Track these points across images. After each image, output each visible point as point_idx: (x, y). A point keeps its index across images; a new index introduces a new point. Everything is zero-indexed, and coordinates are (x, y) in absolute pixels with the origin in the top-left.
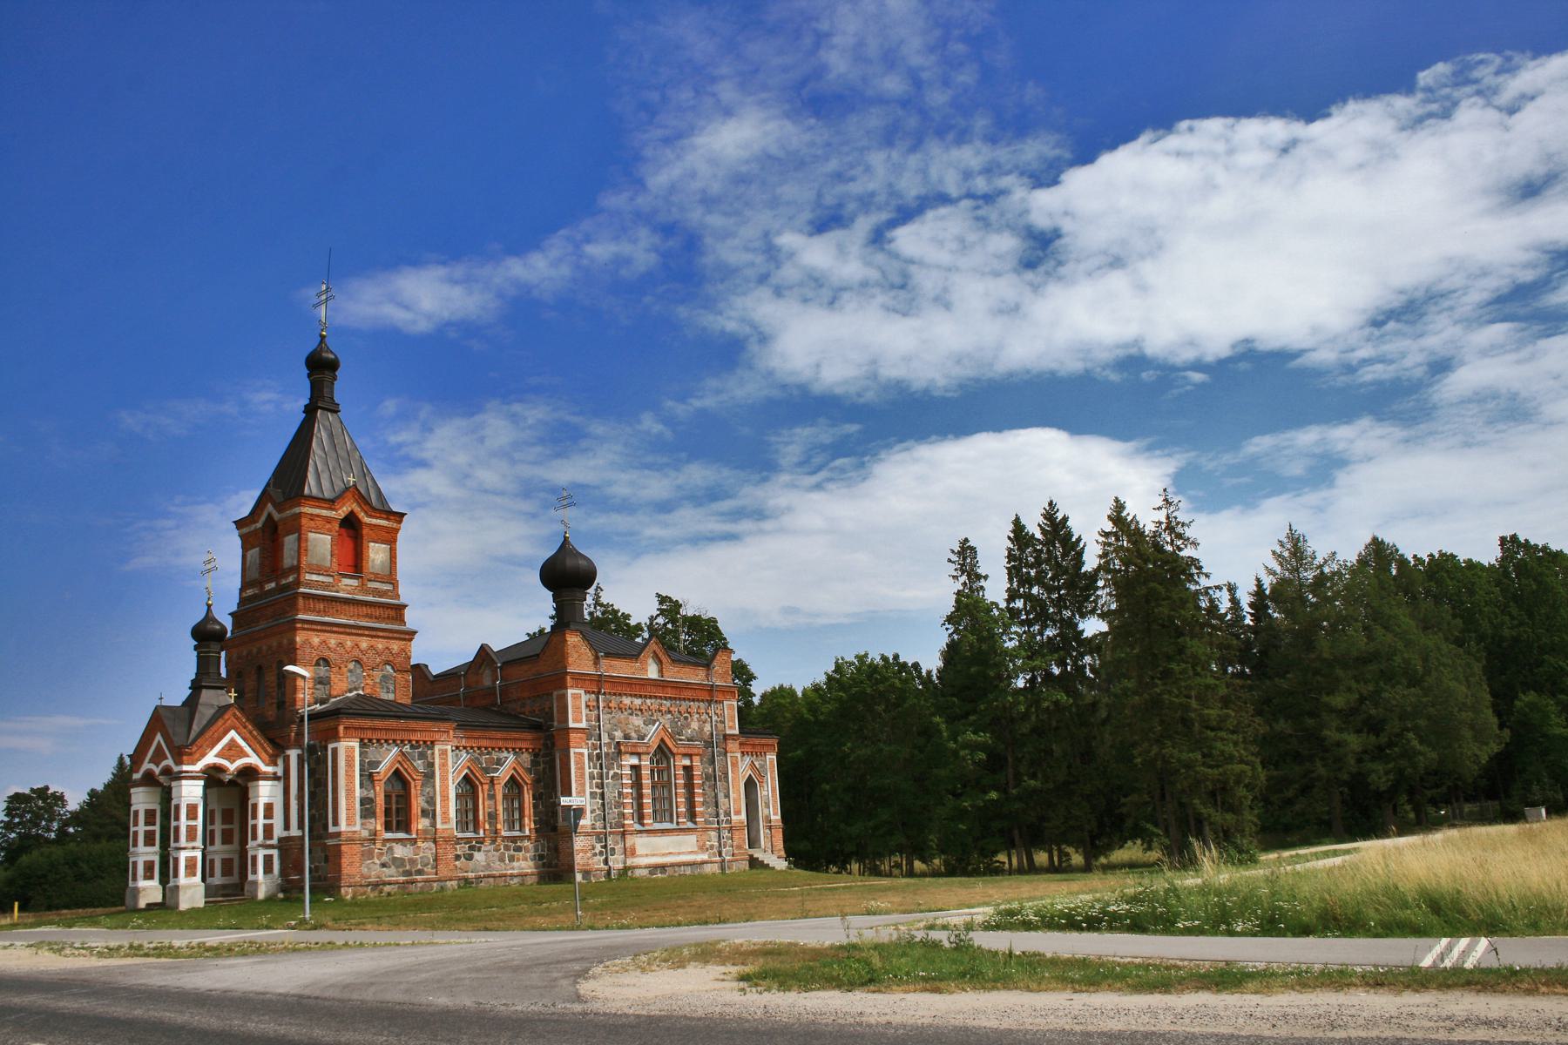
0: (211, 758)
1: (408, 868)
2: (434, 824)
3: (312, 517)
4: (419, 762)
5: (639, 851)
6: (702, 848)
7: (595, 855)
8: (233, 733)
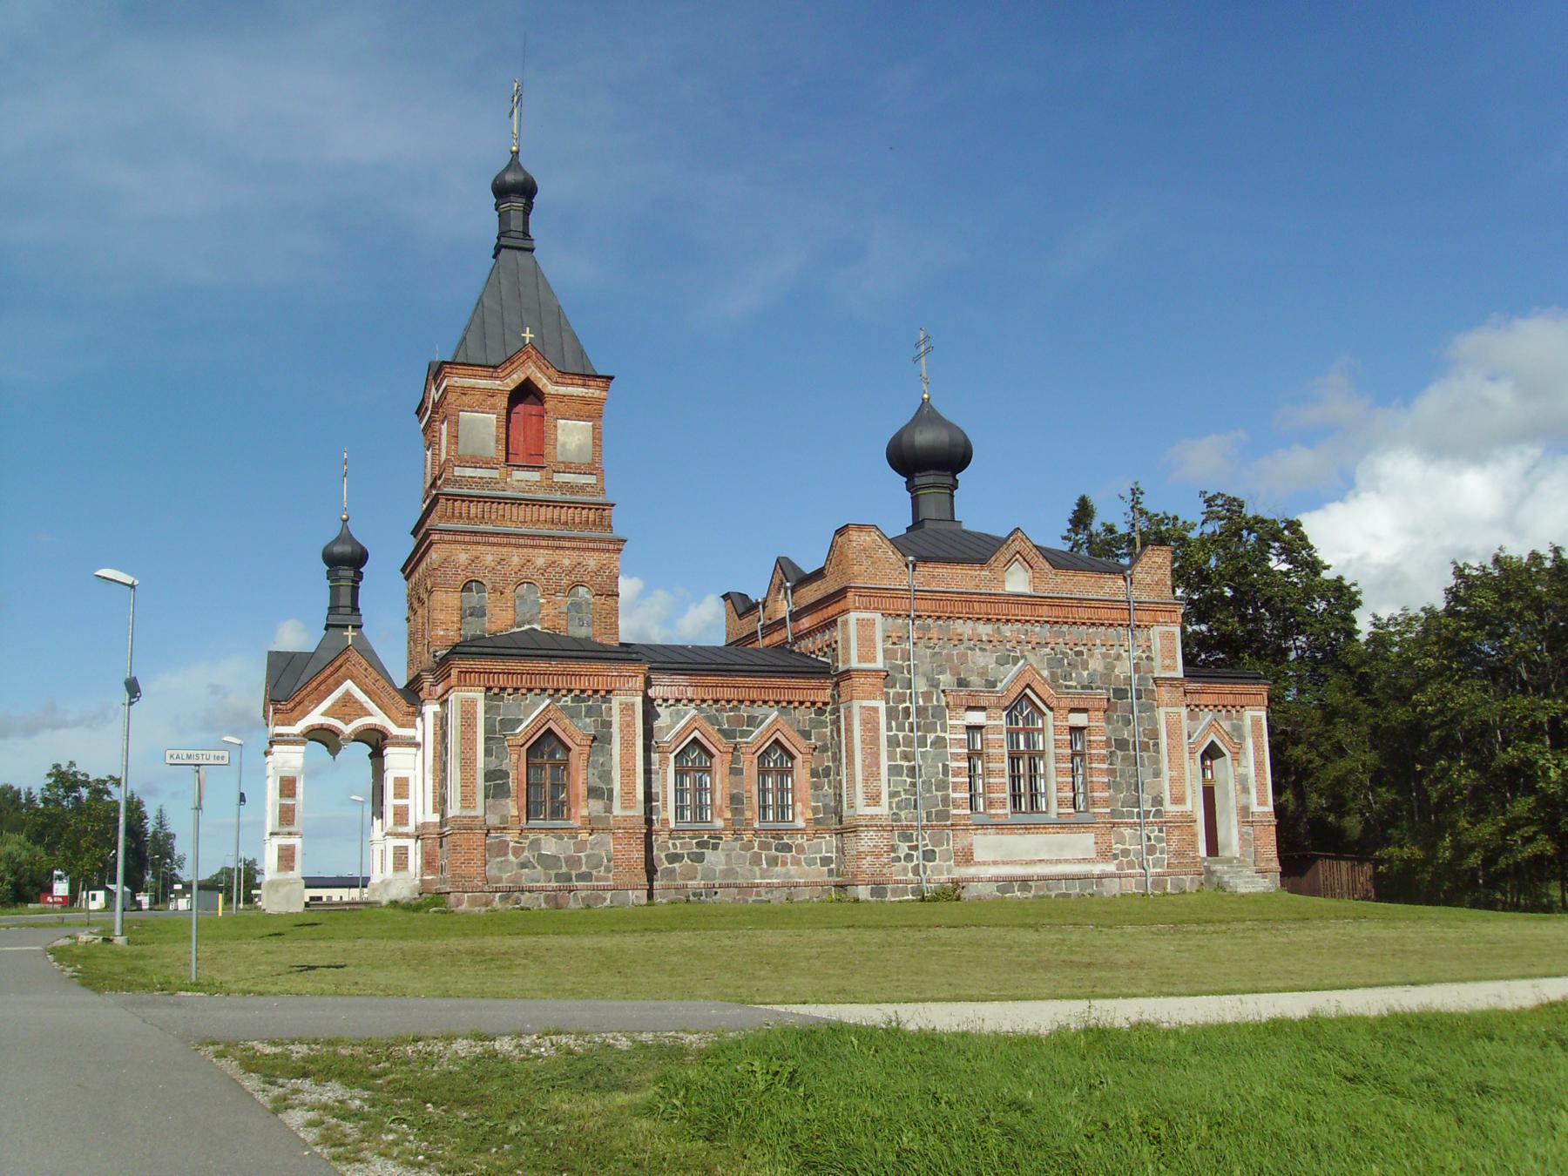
1: (564, 870)
2: (609, 810)
3: (464, 391)
4: (588, 720)
5: (978, 855)
6: (1105, 854)
7: (898, 859)
8: (348, 684)
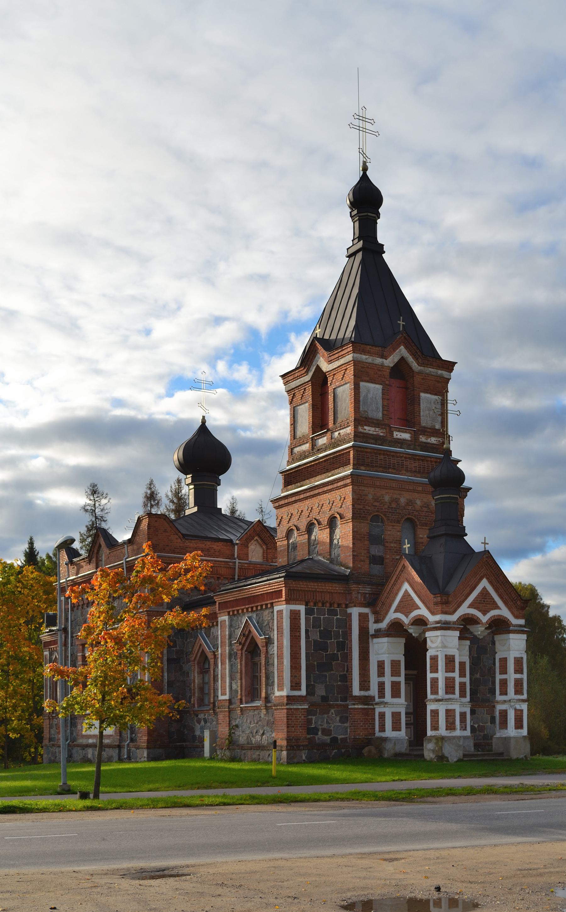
0: (464, 609)
